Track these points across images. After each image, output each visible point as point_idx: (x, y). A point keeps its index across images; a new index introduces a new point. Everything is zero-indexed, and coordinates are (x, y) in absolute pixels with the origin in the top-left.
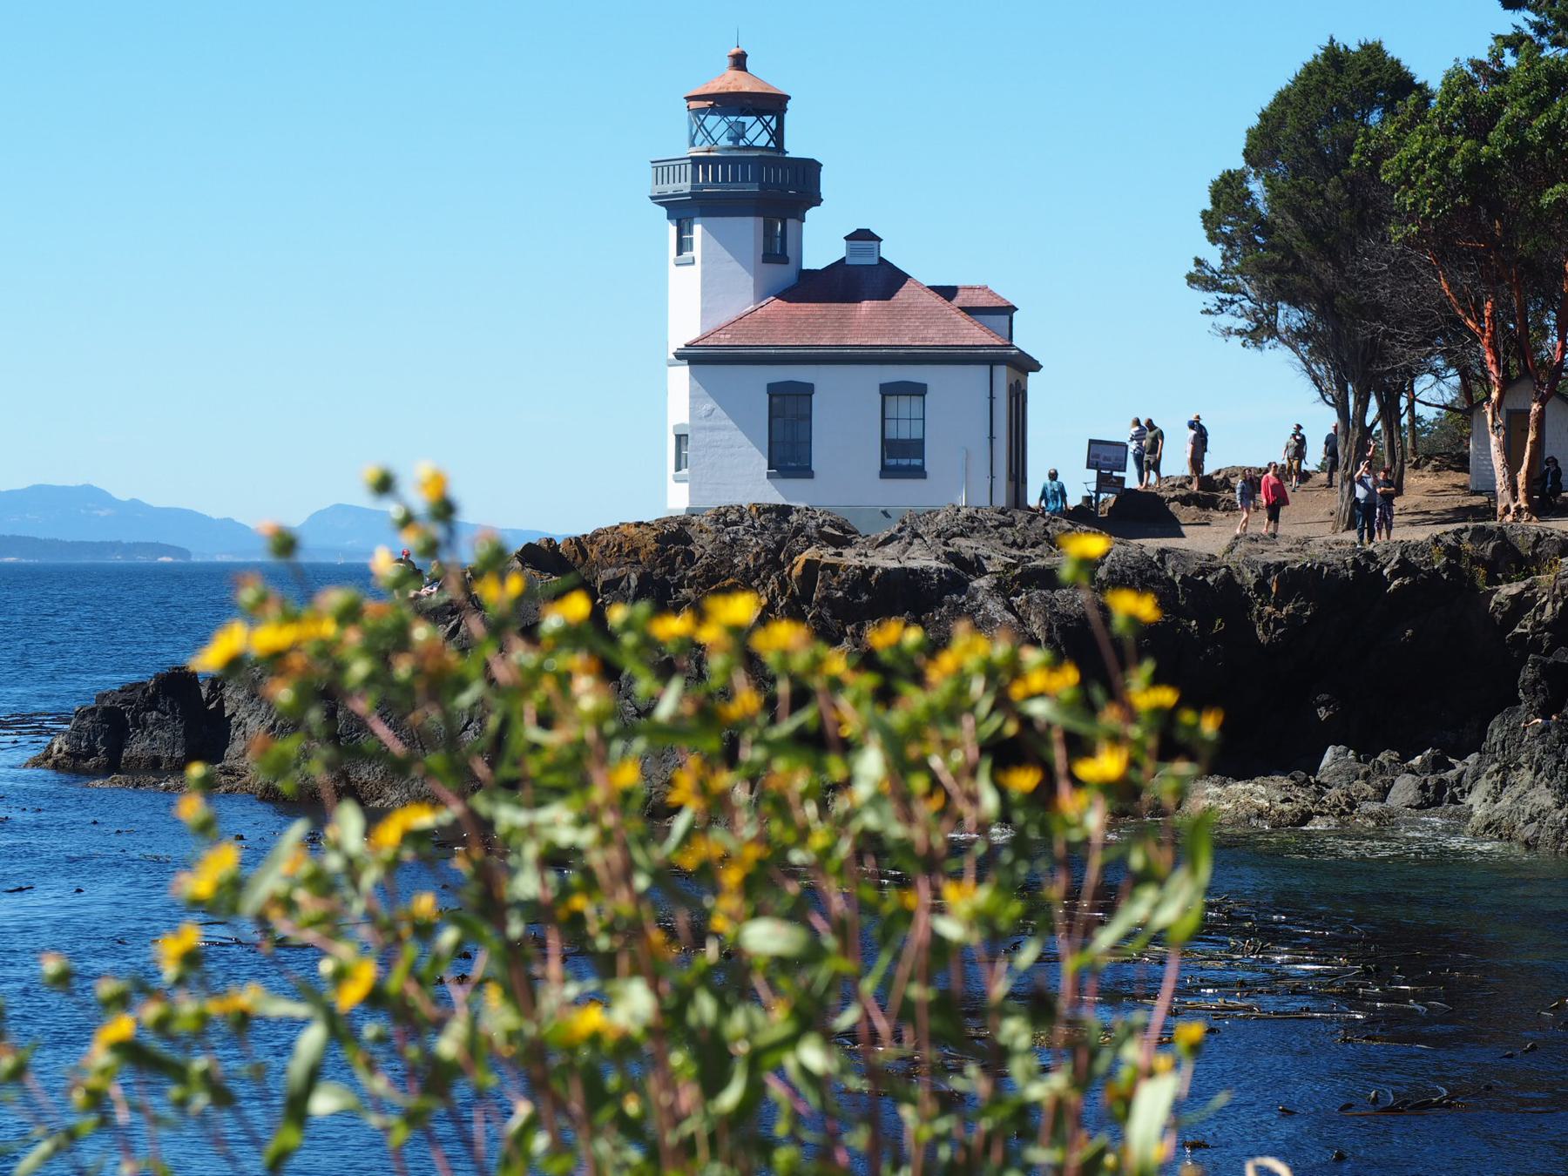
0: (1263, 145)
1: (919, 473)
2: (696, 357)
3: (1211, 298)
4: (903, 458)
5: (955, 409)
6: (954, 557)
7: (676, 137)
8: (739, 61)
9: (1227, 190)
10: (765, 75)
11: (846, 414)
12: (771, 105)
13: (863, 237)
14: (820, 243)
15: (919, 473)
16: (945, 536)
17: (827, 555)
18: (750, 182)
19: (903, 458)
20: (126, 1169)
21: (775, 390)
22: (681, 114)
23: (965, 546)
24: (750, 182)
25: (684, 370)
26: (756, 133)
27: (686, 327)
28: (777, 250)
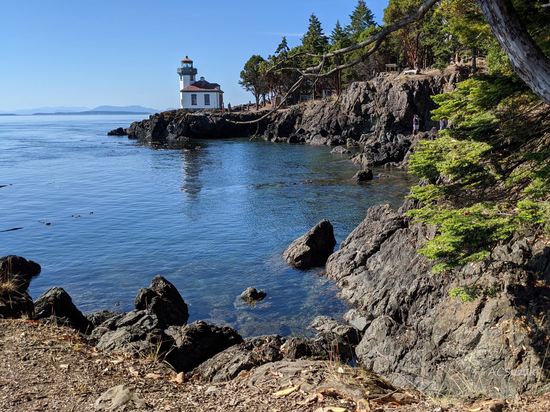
0: (246, 68)
1: (209, 104)
2: (182, 91)
3: (241, 85)
4: (207, 102)
5: (214, 97)
6: (206, 114)
7: (181, 66)
8: (187, 57)
9: (242, 73)
10: (190, 58)
11: (200, 97)
12: (191, 62)
13: (202, 77)
14: (197, 78)
15: (209, 104)
16: (205, 112)
17: (190, 114)
18: (188, 71)
19: (207, 102)
20: (275, 410)
21: (205, 95)
22: (180, 63)
23: (207, 113)
24: (188, 71)
25: (181, 93)
26: (189, 65)
27: (182, 88)
28: (192, 79)
